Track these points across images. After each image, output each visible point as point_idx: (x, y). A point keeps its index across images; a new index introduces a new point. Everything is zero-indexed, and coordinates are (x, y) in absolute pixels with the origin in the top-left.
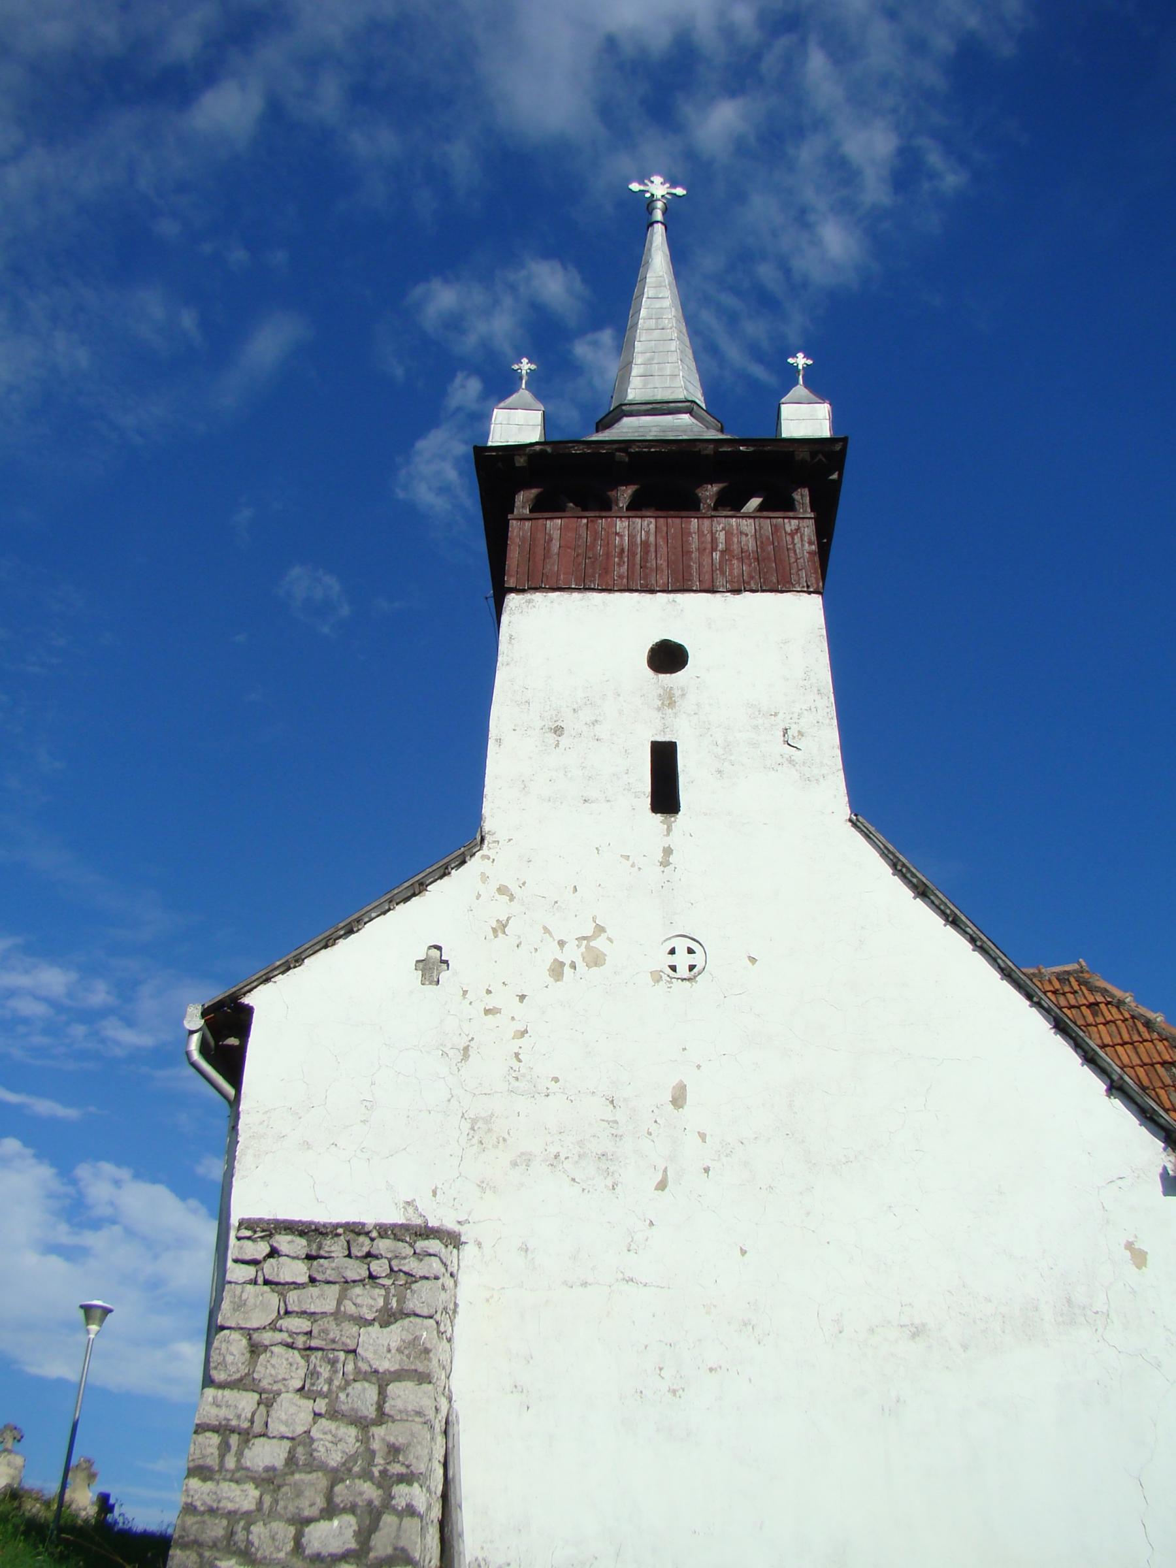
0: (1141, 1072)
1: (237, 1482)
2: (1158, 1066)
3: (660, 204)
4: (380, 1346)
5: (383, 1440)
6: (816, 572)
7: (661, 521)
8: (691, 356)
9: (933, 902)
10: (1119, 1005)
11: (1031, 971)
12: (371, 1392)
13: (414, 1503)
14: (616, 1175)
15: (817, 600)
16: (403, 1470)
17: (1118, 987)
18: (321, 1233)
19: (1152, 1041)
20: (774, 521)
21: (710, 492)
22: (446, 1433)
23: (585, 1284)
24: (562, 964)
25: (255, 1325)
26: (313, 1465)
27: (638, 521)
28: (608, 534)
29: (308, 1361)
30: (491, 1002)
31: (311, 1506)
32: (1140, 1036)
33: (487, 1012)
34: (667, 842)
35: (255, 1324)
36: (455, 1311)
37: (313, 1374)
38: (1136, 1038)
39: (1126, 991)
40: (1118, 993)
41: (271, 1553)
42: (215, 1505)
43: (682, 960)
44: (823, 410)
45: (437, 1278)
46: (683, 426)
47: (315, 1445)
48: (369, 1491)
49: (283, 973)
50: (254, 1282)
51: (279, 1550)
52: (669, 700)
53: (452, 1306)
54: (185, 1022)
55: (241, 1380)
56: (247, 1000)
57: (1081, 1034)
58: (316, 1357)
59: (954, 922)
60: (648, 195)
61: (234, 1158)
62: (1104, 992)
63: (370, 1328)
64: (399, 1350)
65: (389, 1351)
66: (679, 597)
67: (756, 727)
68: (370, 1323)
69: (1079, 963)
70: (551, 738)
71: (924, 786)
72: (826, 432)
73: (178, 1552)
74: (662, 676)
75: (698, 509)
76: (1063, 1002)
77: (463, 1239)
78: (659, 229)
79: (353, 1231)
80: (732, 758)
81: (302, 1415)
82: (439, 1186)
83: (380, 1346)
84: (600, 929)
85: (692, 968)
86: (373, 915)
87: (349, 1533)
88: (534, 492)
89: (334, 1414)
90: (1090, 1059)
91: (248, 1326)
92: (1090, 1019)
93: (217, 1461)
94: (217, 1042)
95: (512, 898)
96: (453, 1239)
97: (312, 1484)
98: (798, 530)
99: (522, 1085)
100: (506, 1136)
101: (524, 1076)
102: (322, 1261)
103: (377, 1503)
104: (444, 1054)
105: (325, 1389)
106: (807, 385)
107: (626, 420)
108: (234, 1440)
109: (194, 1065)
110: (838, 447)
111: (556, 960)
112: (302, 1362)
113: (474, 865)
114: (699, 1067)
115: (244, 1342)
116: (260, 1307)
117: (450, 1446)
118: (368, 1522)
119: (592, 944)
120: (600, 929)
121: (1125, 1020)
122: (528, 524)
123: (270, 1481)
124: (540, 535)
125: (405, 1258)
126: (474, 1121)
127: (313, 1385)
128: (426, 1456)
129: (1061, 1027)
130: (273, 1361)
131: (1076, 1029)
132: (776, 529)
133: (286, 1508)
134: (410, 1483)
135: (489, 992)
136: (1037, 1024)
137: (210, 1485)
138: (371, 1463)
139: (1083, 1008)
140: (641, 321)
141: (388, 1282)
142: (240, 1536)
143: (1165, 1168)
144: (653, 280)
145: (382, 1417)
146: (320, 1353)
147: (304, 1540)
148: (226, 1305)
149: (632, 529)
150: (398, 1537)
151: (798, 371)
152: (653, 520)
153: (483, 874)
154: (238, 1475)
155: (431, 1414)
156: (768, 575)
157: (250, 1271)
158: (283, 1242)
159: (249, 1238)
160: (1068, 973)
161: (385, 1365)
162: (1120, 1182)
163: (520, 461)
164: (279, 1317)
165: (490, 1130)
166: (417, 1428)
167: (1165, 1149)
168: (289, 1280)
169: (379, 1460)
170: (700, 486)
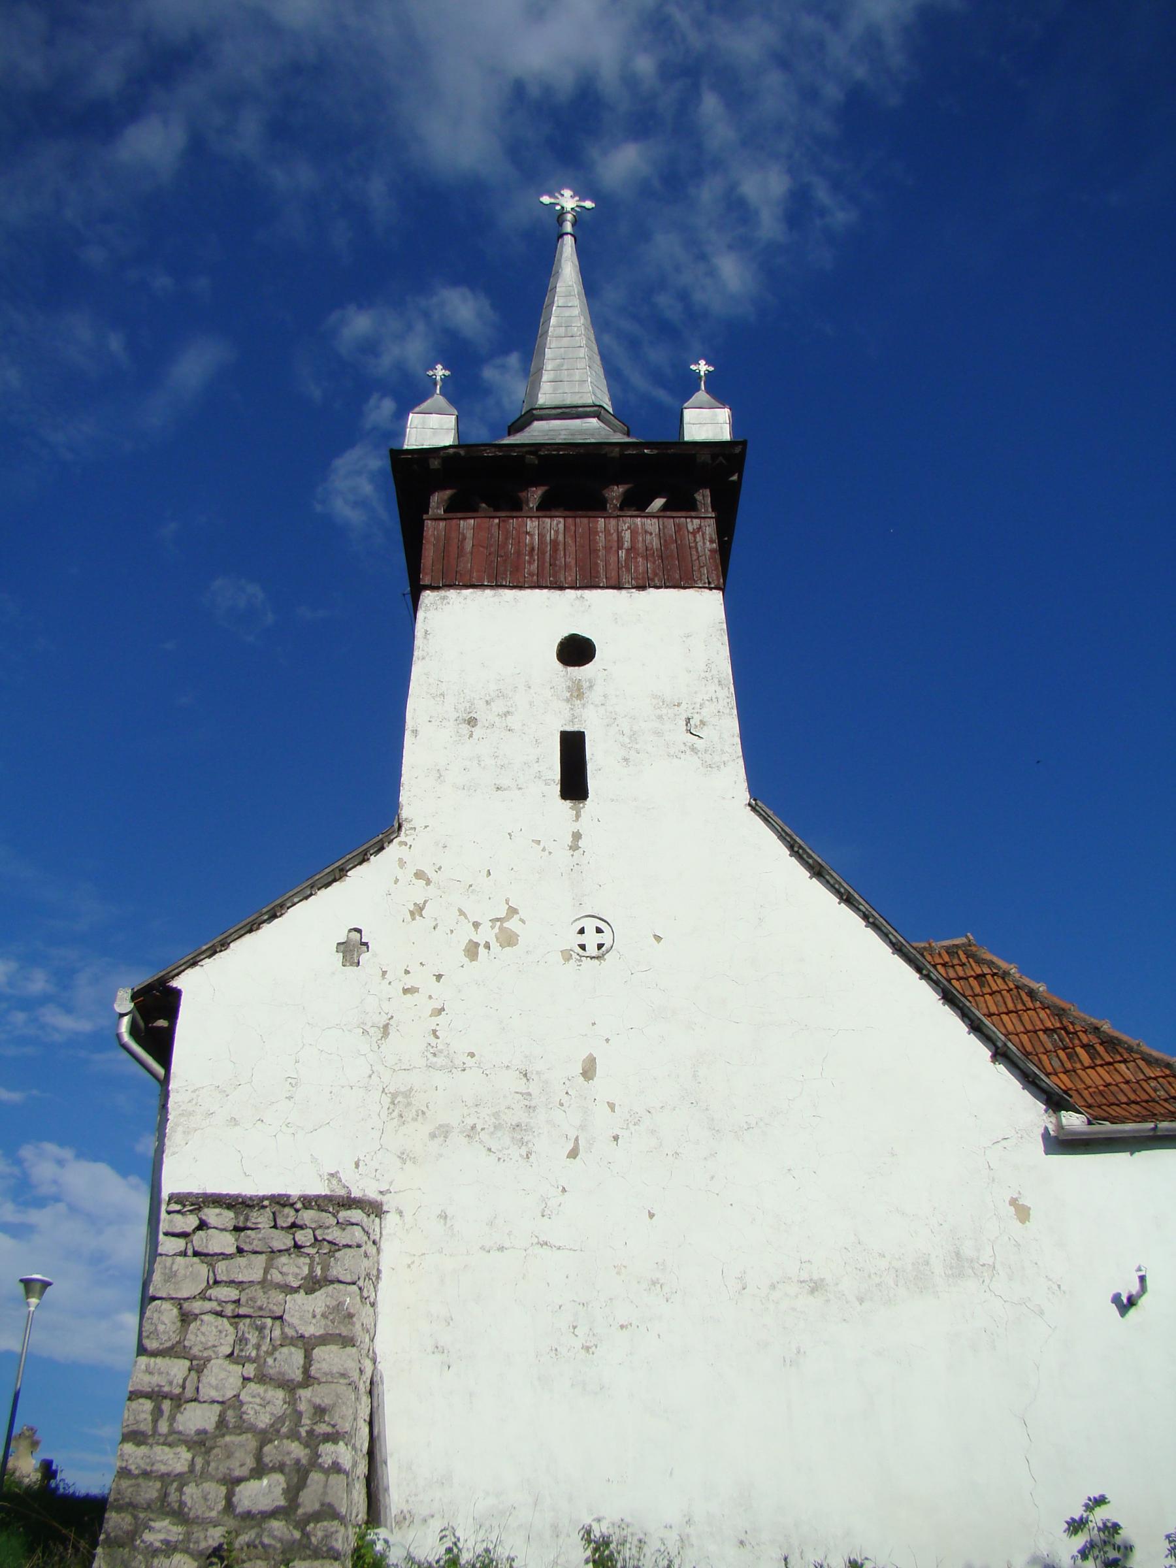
0: (1024, 1038)
1: (170, 1445)
2: (1040, 1033)
3: (569, 217)
4: (306, 1312)
5: (310, 1401)
6: (716, 569)
7: (570, 520)
9: (828, 882)
10: (1005, 975)
11: (922, 945)
12: (298, 1356)
13: (340, 1461)
14: (530, 1145)
15: (718, 595)
16: (329, 1429)
17: (1004, 959)
18: (248, 1206)
19: (1034, 1009)
20: (677, 520)
21: (616, 492)
22: (370, 1393)
23: (501, 1249)
24: (477, 945)
25: (185, 1296)
26: (243, 1427)
27: (548, 520)
30: (409, 982)
31: (241, 1466)
32: (1024, 1005)
33: (406, 991)
34: (575, 827)
35: (185, 1294)
36: (378, 1277)
37: (241, 1340)
38: (1020, 1007)
40: (1003, 965)
42: (149, 1469)
43: (591, 939)
44: (724, 414)
46: (590, 429)
47: (244, 1408)
48: (297, 1450)
49: (210, 956)
50: (184, 1254)
51: (212, 1509)
52: (577, 692)
53: (375, 1272)
55: (172, 1347)
58: (244, 1325)
59: (847, 900)
60: (558, 208)
61: (164, 1135)
62: (990, 964)
63: (296, 1295)
64: (324, 1315)
65: (314, 1316)
66: (587, 593)
67: (660, 717)
68: (295, 1290)
69: (967, 937)
70: (465, 729)
71: (819, 773)
72: (725, 435)
73: (114, 1514)
74: (570, 669)
75: (604, 509)
76: (952, 974)
77: (385, 1208)
78: (569, 241)
79: (278, 1203)
80: (637, 746)
81: (231, 1380)
82: (362, 1158)
83: (306, 1312)
84: (513, 911)
85: (600, 946)
86: (296, 900)
87: (278, 1491)
88: (448, 493)
89: (262, 1378)
90: (976, 1027)
91: (179, 1296)
92: (977, 990)
94: (146, 1024)
95: (428, 882)
96: (375, 1209)
97: (242, 1446)
98: (700, 528)
99: (440, 1061)
100: (425, 1109)
101: (441, 1051)
102: (249, 1232)
103: (304, 1461)
104: (365, 1032)
106: (708, 391)
107: (536, 424)
108: (166, 1405)
109: (125, 1047)
110: (738, 450)
111: (471, 941)
112: (231, 1329)
113: (392, 851)
114: (607, 1040)
115: (175, 1311)
116: (189, 1278)
117: (375, 1405)
118: (296, 1480)
119: (506, 925)
120: (513, 911)
121: (1009, 991)
122: (442, 524)
123: (202, 1443)
124: (454, 535)
125: (328, 1228)
126: (394, 1096)
127: (242, 1350)
129: (949, 998)
130: (203, 1329)
132: (679, 528)
133: (217, 1469)
134: (335, 1442)
135: (407, 972)
137: (143, 1449)
138: (298, 1423)
139: (971, 979)
141: (312, 1251)
142: (173, 1497)
143: (1046, 1129)
144: (563, 289)
145: (308, 1379)
146: (248, 1320)
147: (235, 1499)
148: (157, 1277)
149: (542, 529)
150: (325, 1493)
151: (700, 378)
152: (562, 520)
153: (400, 860)
154: (170, 1439)
155: (355, 1375)
156: (673, 573)
157: (180, 1244)
158: (212, 1215)
159: (178, 1212)
162: (1004, 1143)
163: (435, 464)
164: (209, 1287)
165: (409, 1104)
167: (1046, 1111)
169: (306, 1421)
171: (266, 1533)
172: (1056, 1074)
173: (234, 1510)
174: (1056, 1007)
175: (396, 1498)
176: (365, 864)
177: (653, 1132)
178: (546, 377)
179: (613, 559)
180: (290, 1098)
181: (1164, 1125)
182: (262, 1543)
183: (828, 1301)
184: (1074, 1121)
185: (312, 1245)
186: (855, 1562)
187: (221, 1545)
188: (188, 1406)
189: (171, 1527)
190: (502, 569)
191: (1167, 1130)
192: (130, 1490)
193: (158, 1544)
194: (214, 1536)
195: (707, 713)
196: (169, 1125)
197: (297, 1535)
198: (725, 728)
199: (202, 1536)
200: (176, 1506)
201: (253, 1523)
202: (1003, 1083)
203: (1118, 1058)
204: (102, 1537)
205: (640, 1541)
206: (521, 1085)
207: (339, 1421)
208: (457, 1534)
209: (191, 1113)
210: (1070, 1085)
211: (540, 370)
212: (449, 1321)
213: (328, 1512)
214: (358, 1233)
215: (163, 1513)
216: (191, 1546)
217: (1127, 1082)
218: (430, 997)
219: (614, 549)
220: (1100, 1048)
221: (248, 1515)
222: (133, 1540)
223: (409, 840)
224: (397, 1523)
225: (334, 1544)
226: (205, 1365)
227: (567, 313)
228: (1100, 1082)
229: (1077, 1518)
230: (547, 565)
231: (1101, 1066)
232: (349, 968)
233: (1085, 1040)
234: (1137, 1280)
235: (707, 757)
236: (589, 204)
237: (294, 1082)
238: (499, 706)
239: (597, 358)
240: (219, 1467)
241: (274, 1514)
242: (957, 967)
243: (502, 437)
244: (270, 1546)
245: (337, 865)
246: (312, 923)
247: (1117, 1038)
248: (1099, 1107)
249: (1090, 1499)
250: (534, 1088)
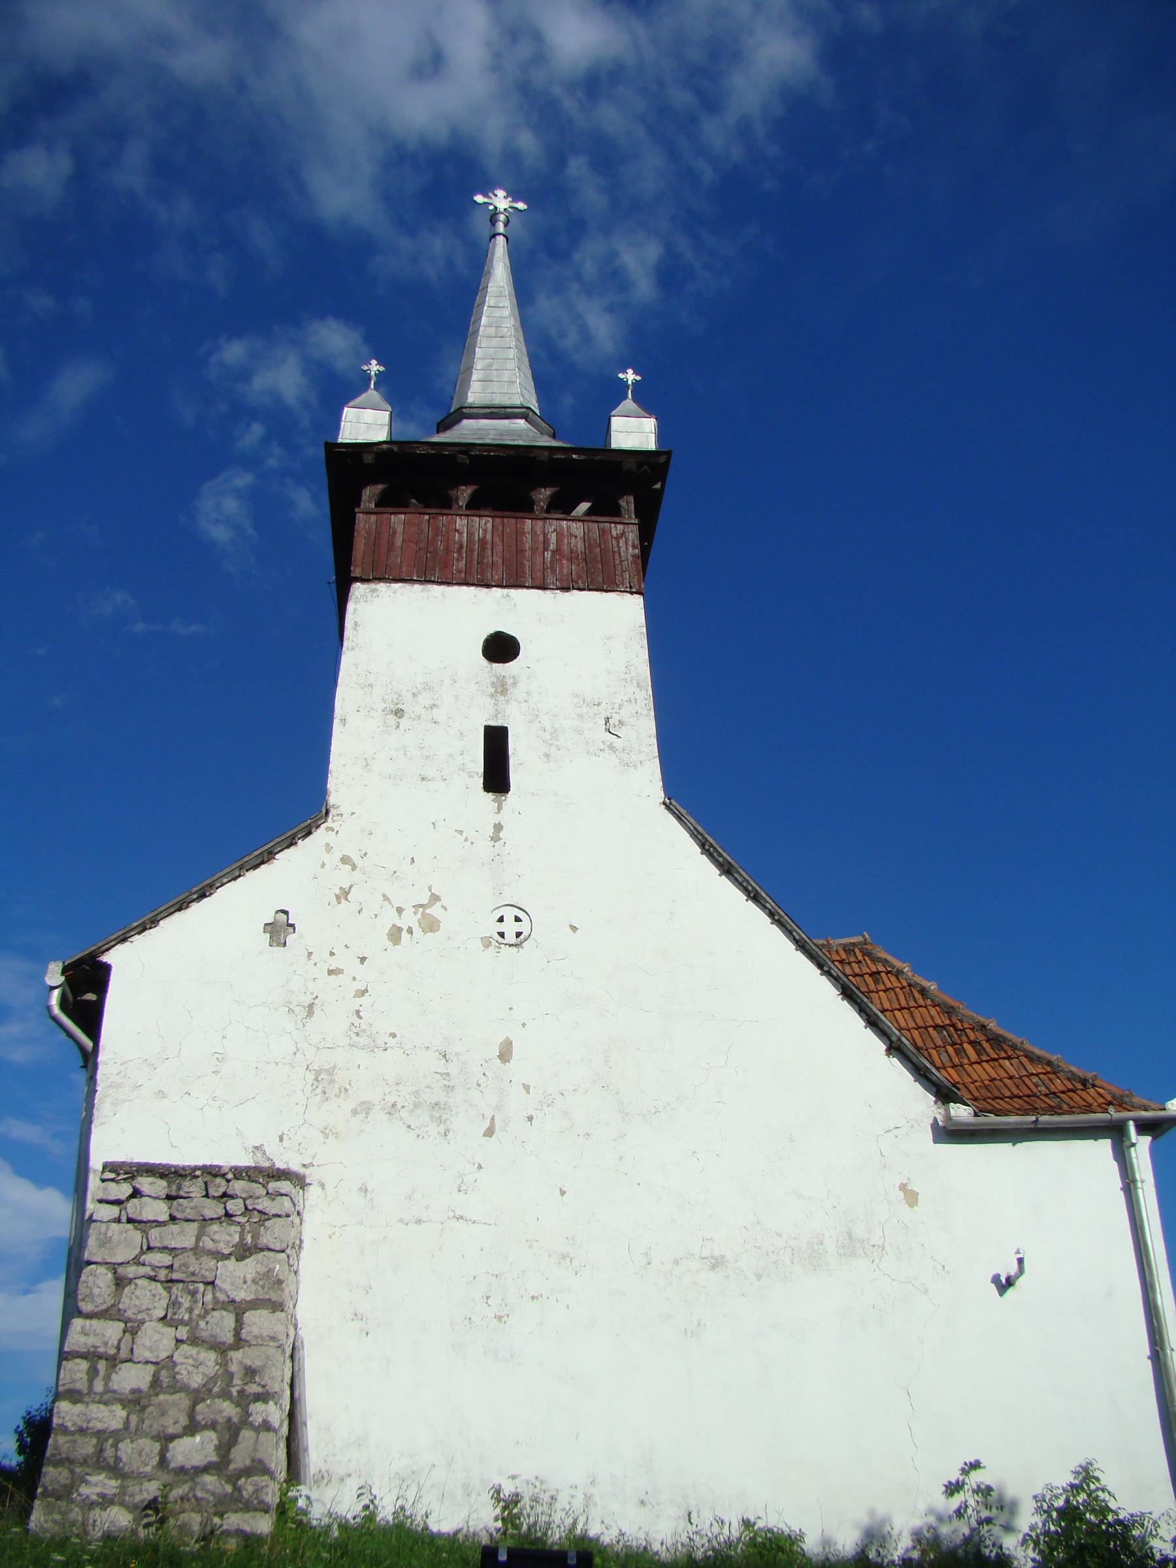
0: (915, 1033)
1: (105, 1404)
2: (931, 1029)
3: (502, 217)
4: (237, 1278)
5: (241, 1363)
6: (638, 575)
7: (498, 520)
8: (527, 364)
9: (736, 879)
10: (898, 974)
11: (821, 942)
12: (229, 1320)
13: (270, 1419)
14: (448, 1123)
15: (637, 602)
16: (259, 1390)
17: (898, 959)
18: (181, 1175)
19: (926, 1007)
20: (602, 525)
21: (543, 495)
22: (292, 1357)
23: (419, 1222)
24: (400, 929)
25: (120, 1260)
26: (176, 1387)
27: (477, 519)
28: (448, 531)
29: (170, 1292)
30: (334, 963)
31: (175, 1423)
32: (916, 1001)
33: (331, 972)
34: (497, 819)
35: (120, 1259)
36: (300, 1247)
37: (174, 1304)
38: (912, 1004)
39: (904, 962)
40: (898, 964)
41: (138, 1468)
42: (85, 1426)
43: (510, 927)
44: (650, 424)
45: (288, 1216)
46: (518, 431)
48: (228, 1409)
49: (139, 933)
50: (118, 1220)
51: (146, 1465)
52: (501, 688)
53: (298, 1242)
54: (47, 979)
55: (107, 1310)
56: (106, 958)
57: (866, 1000)
58: (177, 1289)
59: (755, 897)
60: (491, 208)
61: (93, 1106)
62: (885, 962)
63: (227, 1262)
64: (254, 1281)
65: (245, 1282)
66: (513, 592)
67: (580, 716)
68: (227, 1257)
69: (863, 936)
70: (392, 719)
71: (735, 779)
72: (651, 445)
73: (51, 1469)
74: (495, 665)
75: (532, 511)
76: (848, 971)
77: (308, 1181)
78: (501, 240)
79: (210, 1173)
80: (559, 743)
81: (165, 1342)
82: (286, 1132)
83: (237, 1278)
84: (435, 898)
85: (518, 934)
86: (225, 880)
87: (210, 1447)
88: (380, 487)
89: (194, 1340)
90: (872, 1022)
91: (113, 1261)
92: (872, 987)
93: (86, 1385)
94: (75, 997)
95: (354, 867)
96: (300, 1181)
97: (175, 1404)
98: (623, 534)
99: (362, 1040)
100: (348, 1087)
101: (364, 1031)
102: (181, 1201)
103: (235, 1420)
104: (291, 1011)
105: (186, 1317)
107: (465, 422)
108: (102, 1365)
109: (55, 1019)
110: (662, 459)
111: (394, 925)
112: (165, 1294)
113: (320, 836)
114: (524, 1025)
115: (110, 1276)
116: (124, 1244)
117: (296, 1369)
118: (227, 1437)
119: (428, 911)
120: (435, 898)
121: (902, 988)
122: (373, 518)
123: (137, 1402)
125: (258, 1198)
127: (175, 1314)
128: (277, 1378)
129: (847, 994)
130: (138, 1293)
131: (861, 995)
132: (603, 533)
133: (151, 1426)
134: (265, 1401)
135: (332, 954)
136: (827, 991)
137: (79, 1407)
138: (230, 1384)
139: (866, 977)
140: (482, 329)
141: (243, 1220)
142: (109, 1453)
143: (935, 1119)
144: (494, 289)
145: (239, 1342)
146: (181, 1285)
147: (168, 1455)
148: (92, 1242)
149: (471, 527)
150: (255, 1450)
151: (628, 386)
152: (490, 519)
153: (327, 845)
154: (106, 1397)
155: (283, 1338)
156: (595, 575)
157: (114, 1211)
158: (145, 1183)
159: (112, 1180)
160: (854, 944)
161: (242, 1295)
162: (895, 1132)
163: (368, 458)
164: (142, 1252)
165: (332, 1081)
166: (271, 1351)
167: (936, 1103)
168: (151, 1218)
169: (237, 1381)
170: (535, 488)
171: (199, 1487)
172: (944, 1068)
173: (168, 1465)
174: (946, 1005)
175: (315, 1458)
176: (293, 848)
177: (565, 1113)
178: (476, 376)
179: (539, 560)
180: (216, 1073)
181: (1044, 1118)
182: (195, 1496)
183: (727, 1277)
184: (961, 1112)
185: (243, 1214)
186: (748, 1520)
187: (156, 1498)
188: (123, 1366)
189: (106, 1481)
190: (430, 564)
191: (1048, 1123)
192: (67, 1445)
193: (94, 1497)
194: (151, 1489)
195: (626, 713)
196: (98, 1096)
197: (229, 1488)
198: (642, 729)
199: (137, 1489)
200: (112, 1461)
201: (186, 1477)
202: (896, 1072)
203: (1003, 1055)
204: (39, 1490)
205: (552, 1497)
206: (441, 1066)
207: (269, 1382)
208: (374, 1492)
209: (120, 1086)
210: (957, 1079)
211: (470, 369)
212: (368, 1290)
213: (259, 1468)
214: (286, 1202)
215: (99, 1468)
216: (127, 1498)
217: (1011, 1078)
218: (354, 979)
219: (541, 549)
220: (986, 1045)
221: (181, 1470)
222: (71, 1493)
223: (335, 826)
224: (315, 1482)
225: (264, 1497)
226: (139, 1327)
227: (497, 313)
228: (985, 1077)
229: (953, 1481)
230: (475, 563)
231: (987, 1061)
232: (276, 949)
233: (972, 1038)
234: (1016, 1262)
235: (625, 756)
236: (521, 206)
237: (220, 1057)
238: (425, 699)
239: (526, 360)
240: (153, 1424)
241: (206, 1469)
242: (854, 965)
243: (430, 435)
244: (203, 1499)
245: (266, 848)
246: (244, 901)
247: (1002, 1036)
248: (984, 1100)
249: (966, 1464)
250: (453, 1069)
